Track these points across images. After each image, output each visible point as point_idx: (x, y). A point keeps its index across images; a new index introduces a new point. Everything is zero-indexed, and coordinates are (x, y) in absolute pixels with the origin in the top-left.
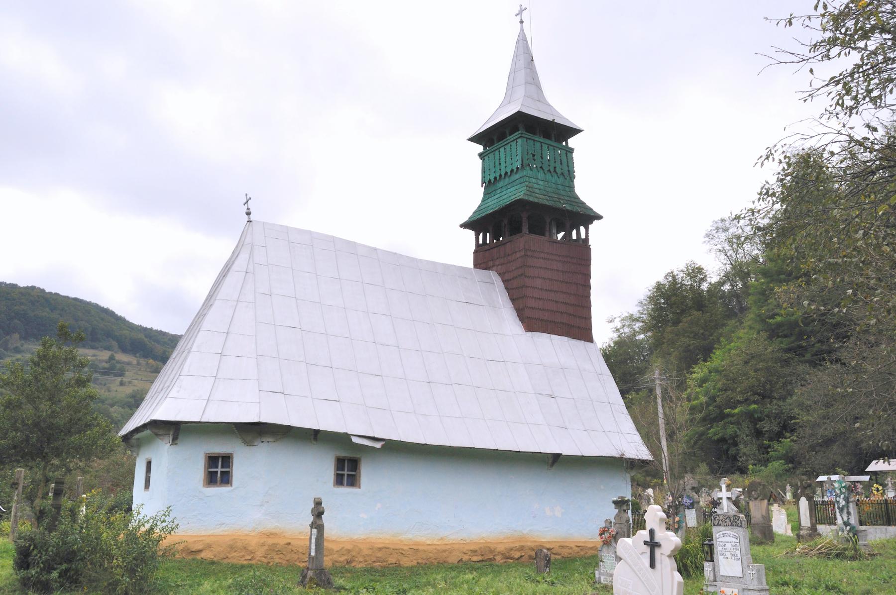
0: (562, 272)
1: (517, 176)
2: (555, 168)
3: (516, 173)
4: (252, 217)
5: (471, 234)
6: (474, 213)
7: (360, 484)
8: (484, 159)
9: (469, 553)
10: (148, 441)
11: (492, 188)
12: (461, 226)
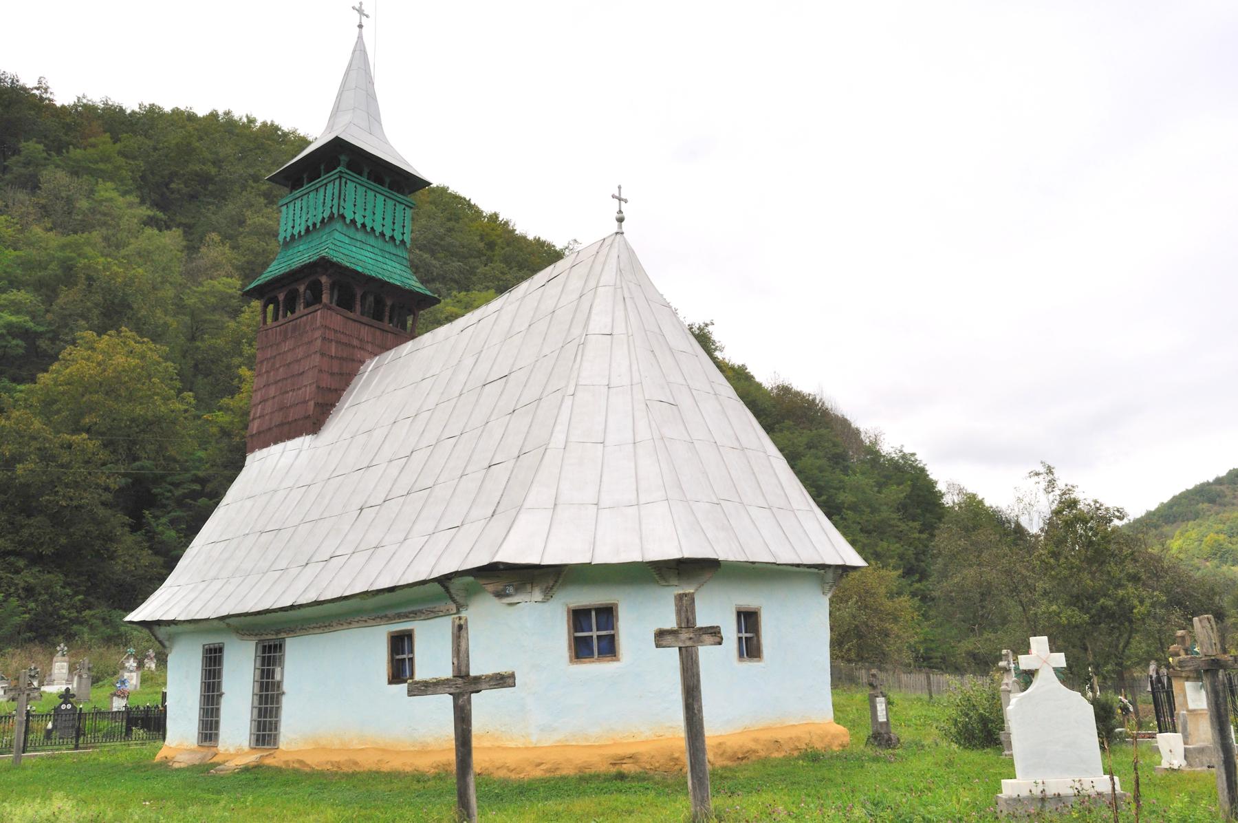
10: (471, 592)
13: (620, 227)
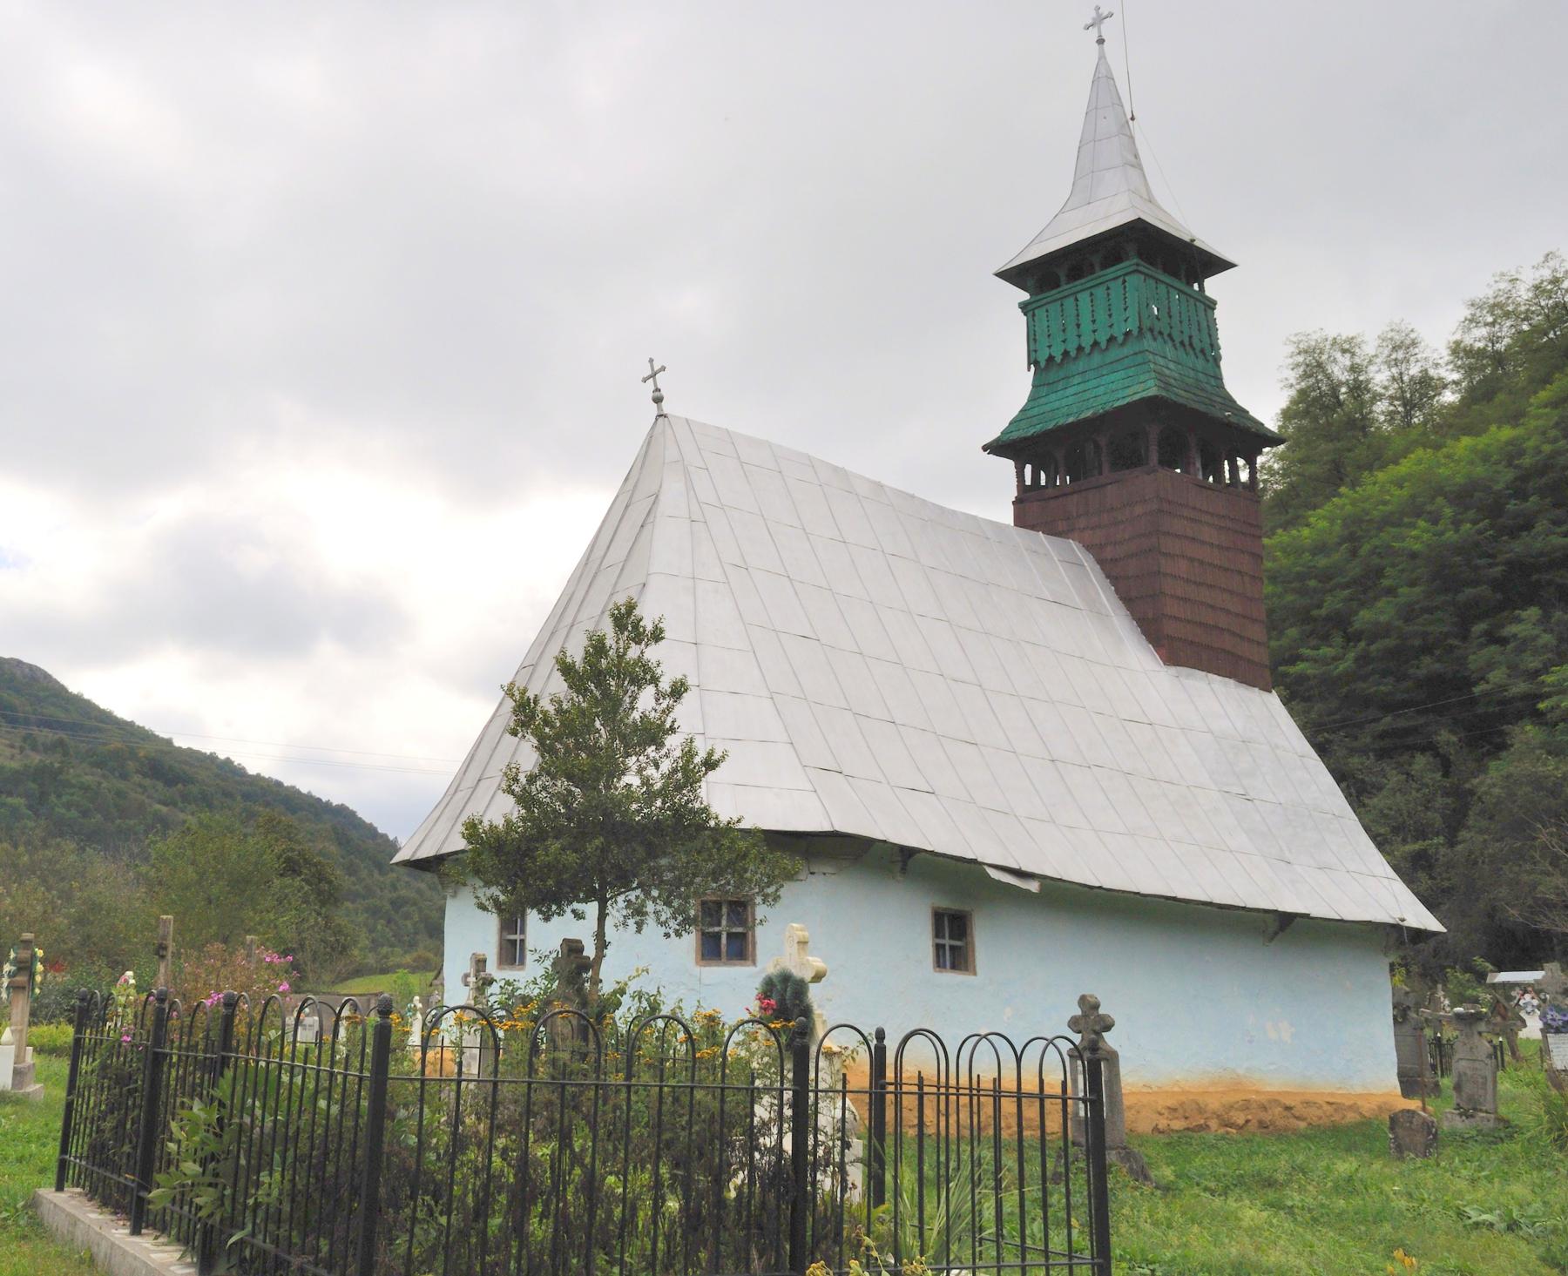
0: (1220, 547)
1: (1126, 351)
2: (1190, 337)
3: (1123, 344)
4: (666, 407)
5: (1008, 465)
6: (1010, 424)
7: (975, 967)
8: (1034, 315)
9: (1166, 1114)
11: (1053, 375)
12: (985, 448)
13: (659, 408)
